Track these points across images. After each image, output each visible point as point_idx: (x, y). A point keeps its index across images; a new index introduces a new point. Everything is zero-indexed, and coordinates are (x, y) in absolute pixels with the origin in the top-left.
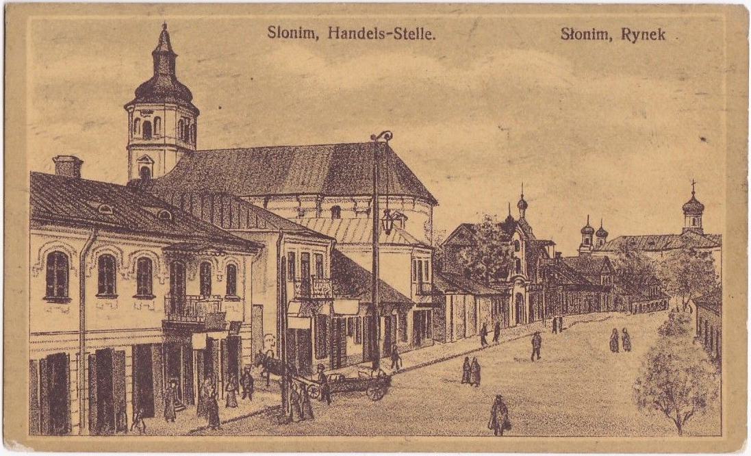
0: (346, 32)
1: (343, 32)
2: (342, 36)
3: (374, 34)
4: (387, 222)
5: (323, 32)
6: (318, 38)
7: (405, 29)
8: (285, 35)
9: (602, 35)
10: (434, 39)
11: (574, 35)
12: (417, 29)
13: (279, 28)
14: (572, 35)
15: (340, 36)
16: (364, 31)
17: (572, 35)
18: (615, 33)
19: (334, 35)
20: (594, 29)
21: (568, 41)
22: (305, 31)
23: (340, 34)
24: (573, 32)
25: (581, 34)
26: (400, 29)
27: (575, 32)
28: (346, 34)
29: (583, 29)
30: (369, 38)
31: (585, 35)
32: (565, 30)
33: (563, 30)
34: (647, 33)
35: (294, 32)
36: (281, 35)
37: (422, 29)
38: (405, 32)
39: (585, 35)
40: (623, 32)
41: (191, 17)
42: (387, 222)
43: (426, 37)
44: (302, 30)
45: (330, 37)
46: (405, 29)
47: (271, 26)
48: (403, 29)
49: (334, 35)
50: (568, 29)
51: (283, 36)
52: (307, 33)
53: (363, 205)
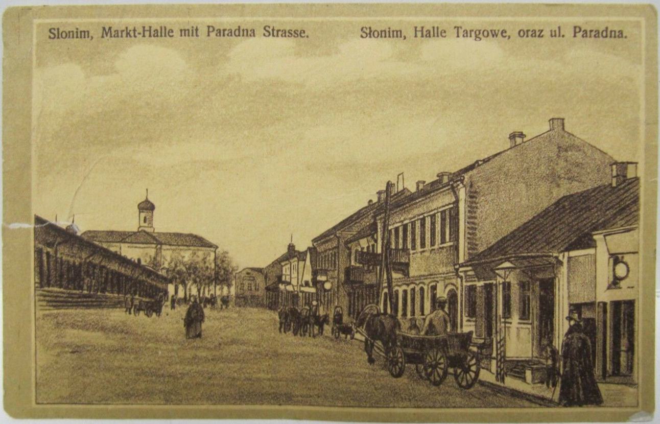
0: (117, 31)
1: (115, 31)
2: (580, 31)
3: (598, 34)
4: (385, 309)
5: (512, 32)
6: (92, 38)
7: (197, 28)
8: (376, 35)
9: (84, 34)
10: (307, 37)
11: (372, 34)
12: (434, 28)
13: (58, 29)
14: (370, 34)
15: (113, 35)
16: (239, 30)
17: (370, 34)
18: (96, 33)
19: (419, 34)
20: (389, 28)
21: (488, 38)
22: (393, 31)
23: (152, 33)
24: (371, 31)
25: (235, 34)
26: (269, 27)
27: (601, 32)
28: (467, 33)
29: (68, 29)
30: (301, 36)
31: (69, 35)
32: (364, 29)
33: (362, 29)
34: (615, 32)
35: (71, 33)
36: (60, 36)
37: (438, 28)
38: (273, 30)
39: (69, 35)
40: (209, 29)
41: (313, 19)
42: (385, 309)
43: (441, 35)
44: (79, 31)
45: (416, 36)
46: (197, 28)
47: (267, 26)
48: (272, 28)
49: (419, 34)
50: (367, 28)
51: (602, 36)
52: (395, 33)
53: (179, 338)
